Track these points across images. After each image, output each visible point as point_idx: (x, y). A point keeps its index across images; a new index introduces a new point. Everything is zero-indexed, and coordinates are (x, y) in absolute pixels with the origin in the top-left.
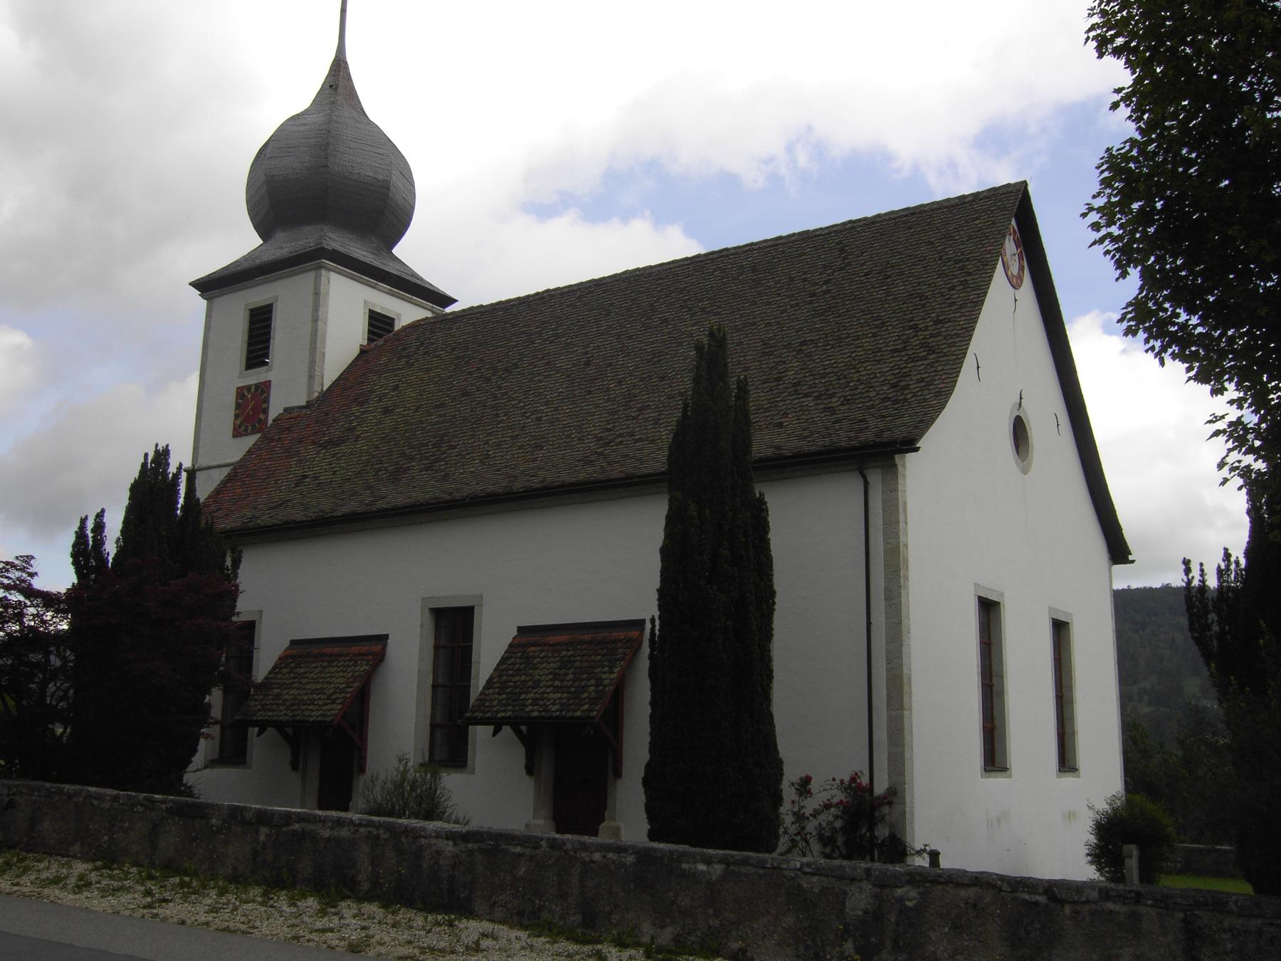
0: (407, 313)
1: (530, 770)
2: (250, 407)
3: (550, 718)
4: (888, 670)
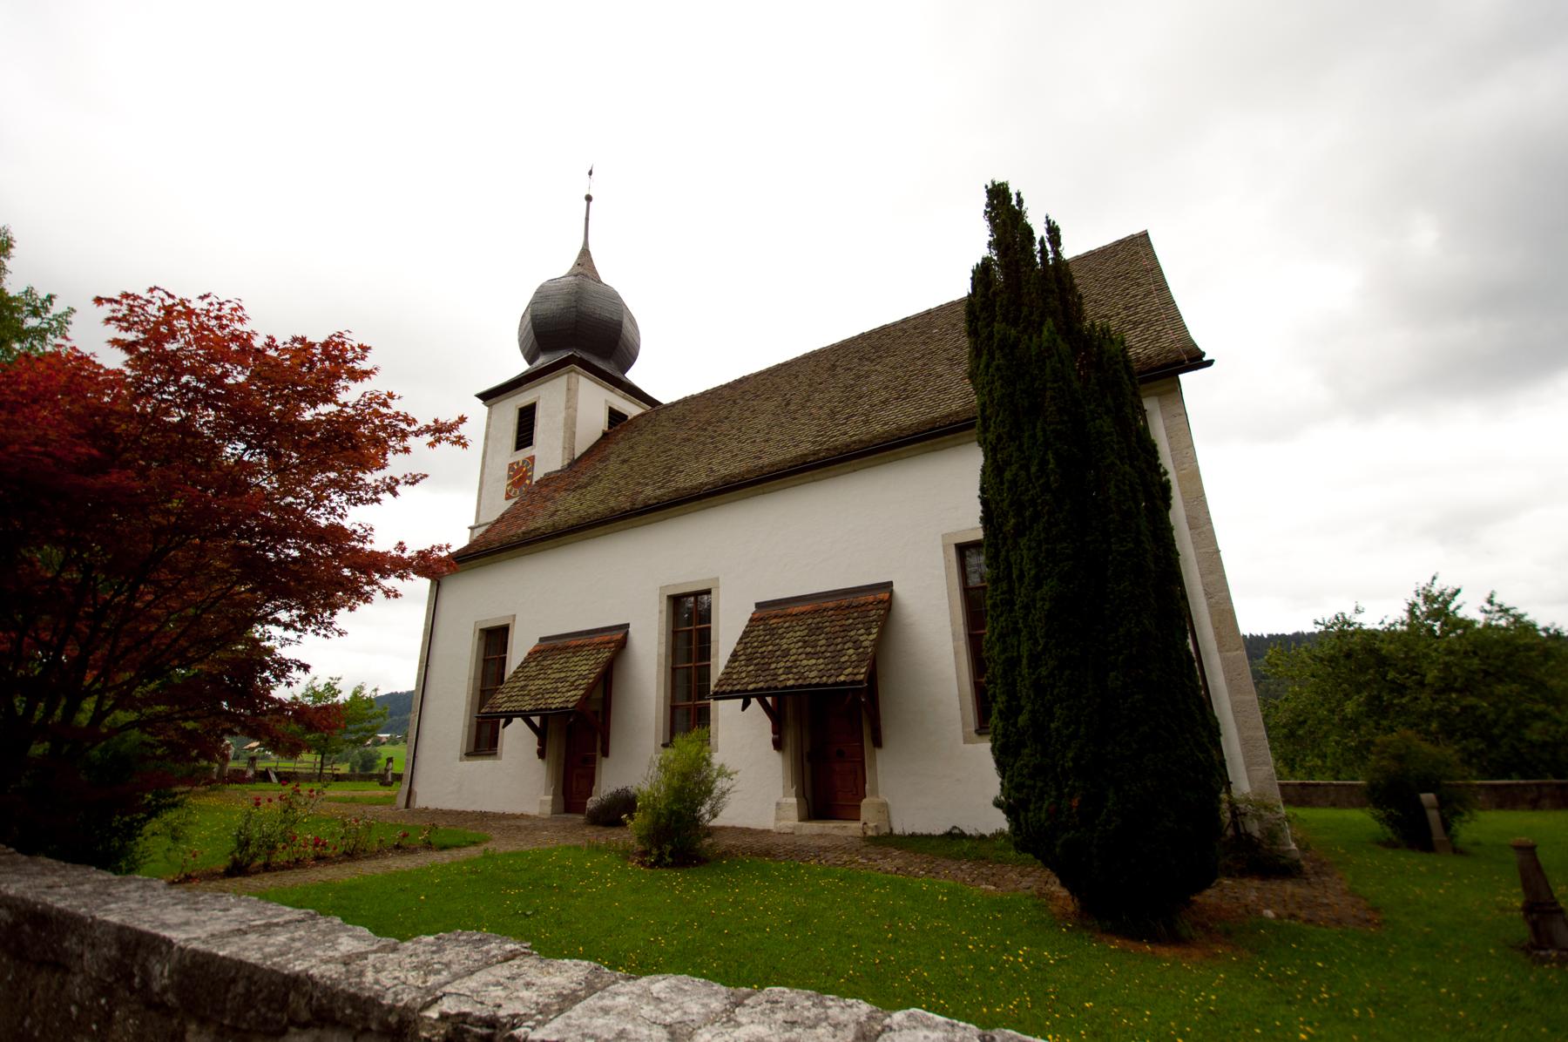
0: (632, 409)
1: (778, 745)
2: (519, 475)
3: (810, 685)
4: (1210, 606)
